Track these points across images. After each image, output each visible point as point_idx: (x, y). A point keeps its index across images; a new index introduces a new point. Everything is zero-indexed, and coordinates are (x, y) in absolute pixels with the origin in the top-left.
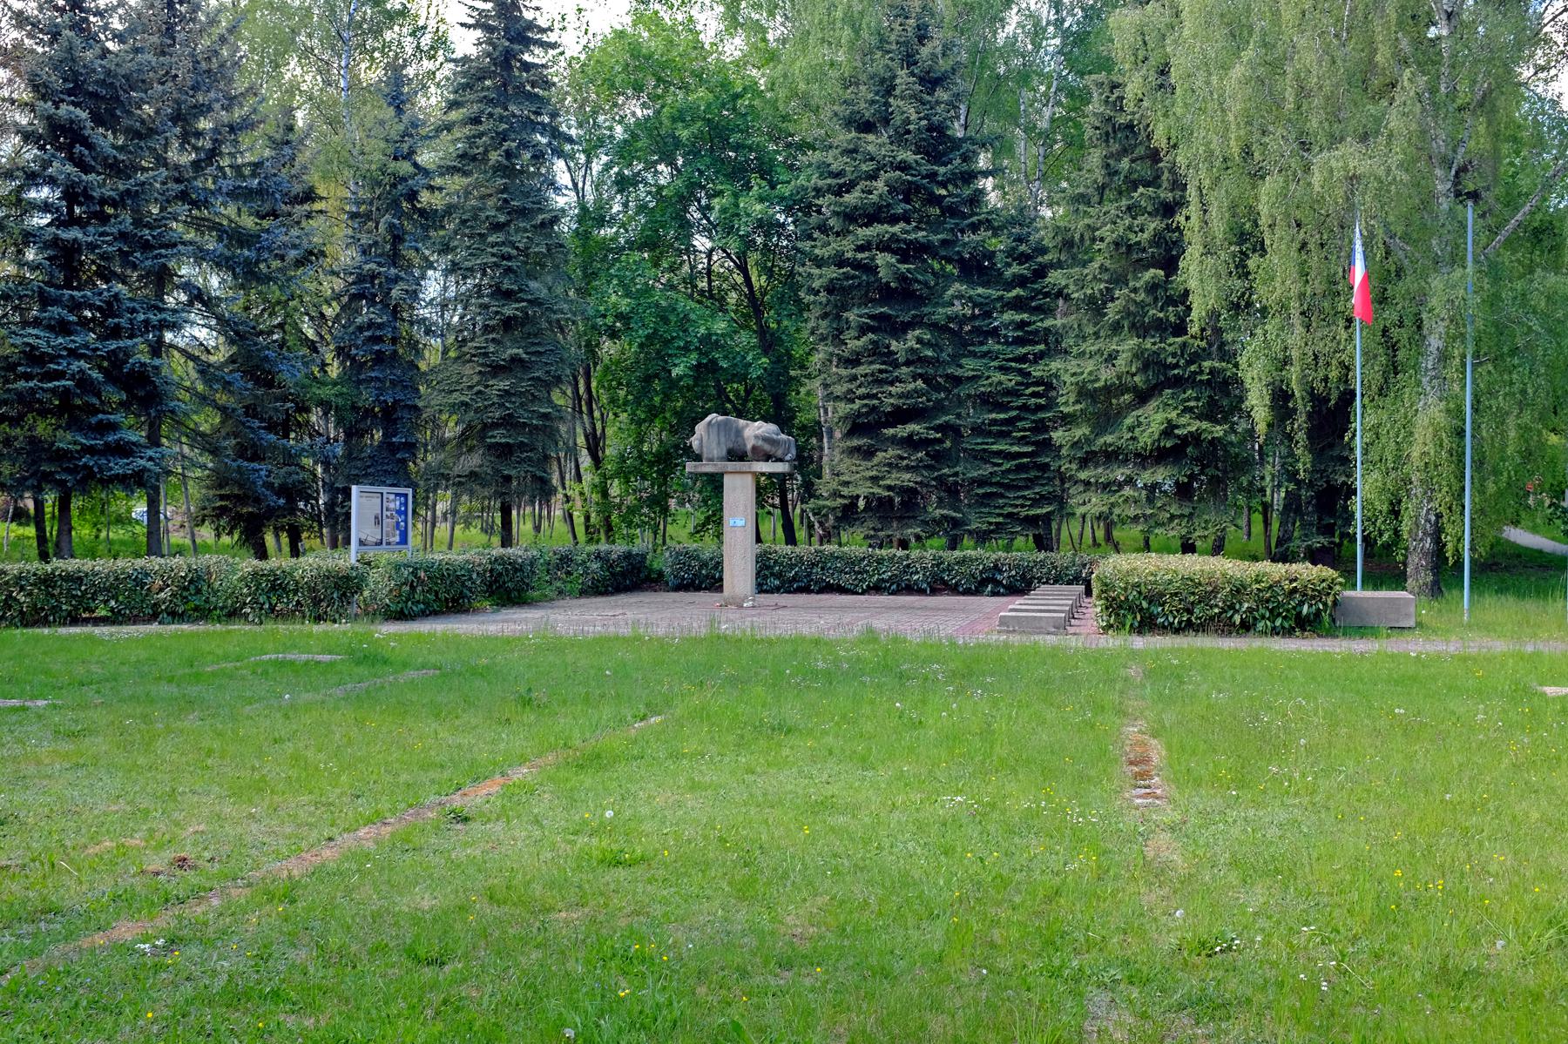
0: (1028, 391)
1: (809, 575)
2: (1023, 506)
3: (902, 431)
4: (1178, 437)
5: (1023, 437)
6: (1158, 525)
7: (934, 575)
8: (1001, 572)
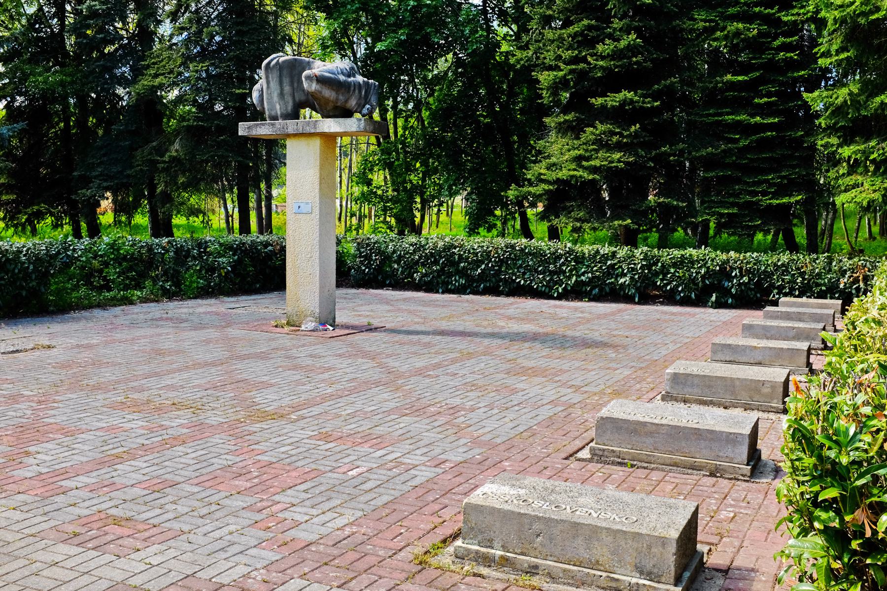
0: (777, 43)
1: (499, 272)
2: (764, 193)
7: (643, 277)
8: (730, 278)
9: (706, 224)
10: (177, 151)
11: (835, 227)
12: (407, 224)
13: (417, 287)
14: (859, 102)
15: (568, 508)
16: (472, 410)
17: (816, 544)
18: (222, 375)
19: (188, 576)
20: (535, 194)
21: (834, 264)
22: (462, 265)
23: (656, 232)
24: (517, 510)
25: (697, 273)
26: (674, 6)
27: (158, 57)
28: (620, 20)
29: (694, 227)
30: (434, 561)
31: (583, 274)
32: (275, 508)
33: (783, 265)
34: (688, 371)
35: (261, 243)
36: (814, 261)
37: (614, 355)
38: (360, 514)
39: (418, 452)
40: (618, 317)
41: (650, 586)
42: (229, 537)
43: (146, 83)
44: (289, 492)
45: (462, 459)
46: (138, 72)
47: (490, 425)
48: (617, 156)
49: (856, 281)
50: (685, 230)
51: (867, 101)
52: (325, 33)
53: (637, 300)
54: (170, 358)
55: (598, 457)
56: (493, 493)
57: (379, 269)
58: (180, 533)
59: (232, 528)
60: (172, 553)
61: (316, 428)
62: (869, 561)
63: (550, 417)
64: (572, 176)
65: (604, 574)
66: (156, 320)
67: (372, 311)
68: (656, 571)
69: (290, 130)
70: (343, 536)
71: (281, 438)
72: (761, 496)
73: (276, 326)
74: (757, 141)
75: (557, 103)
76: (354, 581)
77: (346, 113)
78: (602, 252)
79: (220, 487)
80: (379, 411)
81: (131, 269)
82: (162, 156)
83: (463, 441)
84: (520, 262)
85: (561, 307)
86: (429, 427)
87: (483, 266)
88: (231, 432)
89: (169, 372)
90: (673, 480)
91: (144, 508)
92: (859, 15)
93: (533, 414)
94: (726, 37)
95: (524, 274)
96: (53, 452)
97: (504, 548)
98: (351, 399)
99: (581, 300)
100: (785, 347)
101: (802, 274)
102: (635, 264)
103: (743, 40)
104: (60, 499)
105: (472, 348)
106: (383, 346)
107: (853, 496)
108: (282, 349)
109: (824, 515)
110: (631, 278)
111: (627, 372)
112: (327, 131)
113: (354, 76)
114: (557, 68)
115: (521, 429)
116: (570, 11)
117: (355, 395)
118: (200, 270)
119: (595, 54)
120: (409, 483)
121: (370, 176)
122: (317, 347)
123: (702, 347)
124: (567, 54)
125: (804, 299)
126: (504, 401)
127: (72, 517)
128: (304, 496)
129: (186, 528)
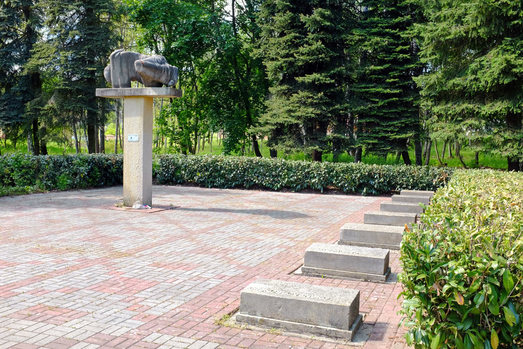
0: (398, 49)
1: (243, 176)
2: (392, 132)
3: (308, 78)
4: (515, 75)
5: (394, 83)
6: (495, 147)
8: (373, 179)
9: (360, 150)
10: (52, 103)
11: (431, 150)
12: (187, 147)
13: (196, 184)
14: (442, 83)
15: (295, 293)
16: (236, 250)
17: (416, 301)
18: (91, 233)
19: (97, 333)
20: (264, 131)
21: (430, 171)
22: (222, 171)
23: (332, 153)
24: (268, 295)
25: (356, 176)
26: (342, 27)
27: (41, 47)
28: (313, 33)
29: (354, 150)
30: (226, 324)
31: (292, 177)
32: (137, 300)
33: (402, 172)
34: (352, 228)
35: (104, 158)
36: (419, 170)
37: (311, 221)
38: (183, 302)
39: (209, 272)
40: (312, 201)
41: (336, 331)
42: (115, 315)
43: (33, 63)
44: (143, 292)
45: (234, 275)
46: (27, 56)
47: (247, 258)
48: (310, 110)
49: (442, 181)
50: (348, 152)
51: (446, 82)
52: (142, 36)
53: (322, 192)
54: (59, 224)
55: (306, 273)
56: (256, 288)
57: (173, 175)
58: (87, 313)
59: (116, 310)
60: (85, 323)
61: (151, 260)
62: (438, 307)
63: (279, 254)
64: (285, 121)
65: (313, 326)
66: (45, 203)
67: (171, 198)
68: (339, 323)
69: (127, 94)
70: (175, 313)
71: (133, 266)
72: (391, 290)
73: (117, 207)
74: (388, 103)
75: (277, 79)
76: (185, 333)
77: (160, 85)
78: (302, 164)
79: (104, 291)
80: (184, 251)
81: (27, 173)
82: (43, 106)
83: (232, 266)
84: (256, 170)
85: (279, 195)
86: (213, 259)
87: (234, 172)
88: (104, 263)
89: (60, 232)
90: (346, 283)
91: (64, 302)
92: (440, 36)
93: (269, 252)
94: (371, 45)
95: (258, 177)
96: (4, 275)
97: (262, 315)
98: (168, 245)
99: (291, 192)
100: (403, 216)
101: (413, 177)
102: (321, 171)
103: (380, 47)
104: (15, 298)
105: (232, 218)
106: (181, 217)
107: (432, 278)
108: (123, 219)
109: (419, 288)
110: (319, 179)
111: (319, 230)
112: (148, 94)
113: (164, 64)
114: (277, 59)
115: (263, 260)
116: (284, 28)
117: (170, 243)
118: (68, 175)
119: (298, 53)
120: (207, 287)
121: (166, 120)
122: (143, 218)
123: (359, 217)
124: (283, 52)
125: (414, 191)
126: (253, 246)
127: (25, 307)
128: (151, 294)
129: (90, 311)
